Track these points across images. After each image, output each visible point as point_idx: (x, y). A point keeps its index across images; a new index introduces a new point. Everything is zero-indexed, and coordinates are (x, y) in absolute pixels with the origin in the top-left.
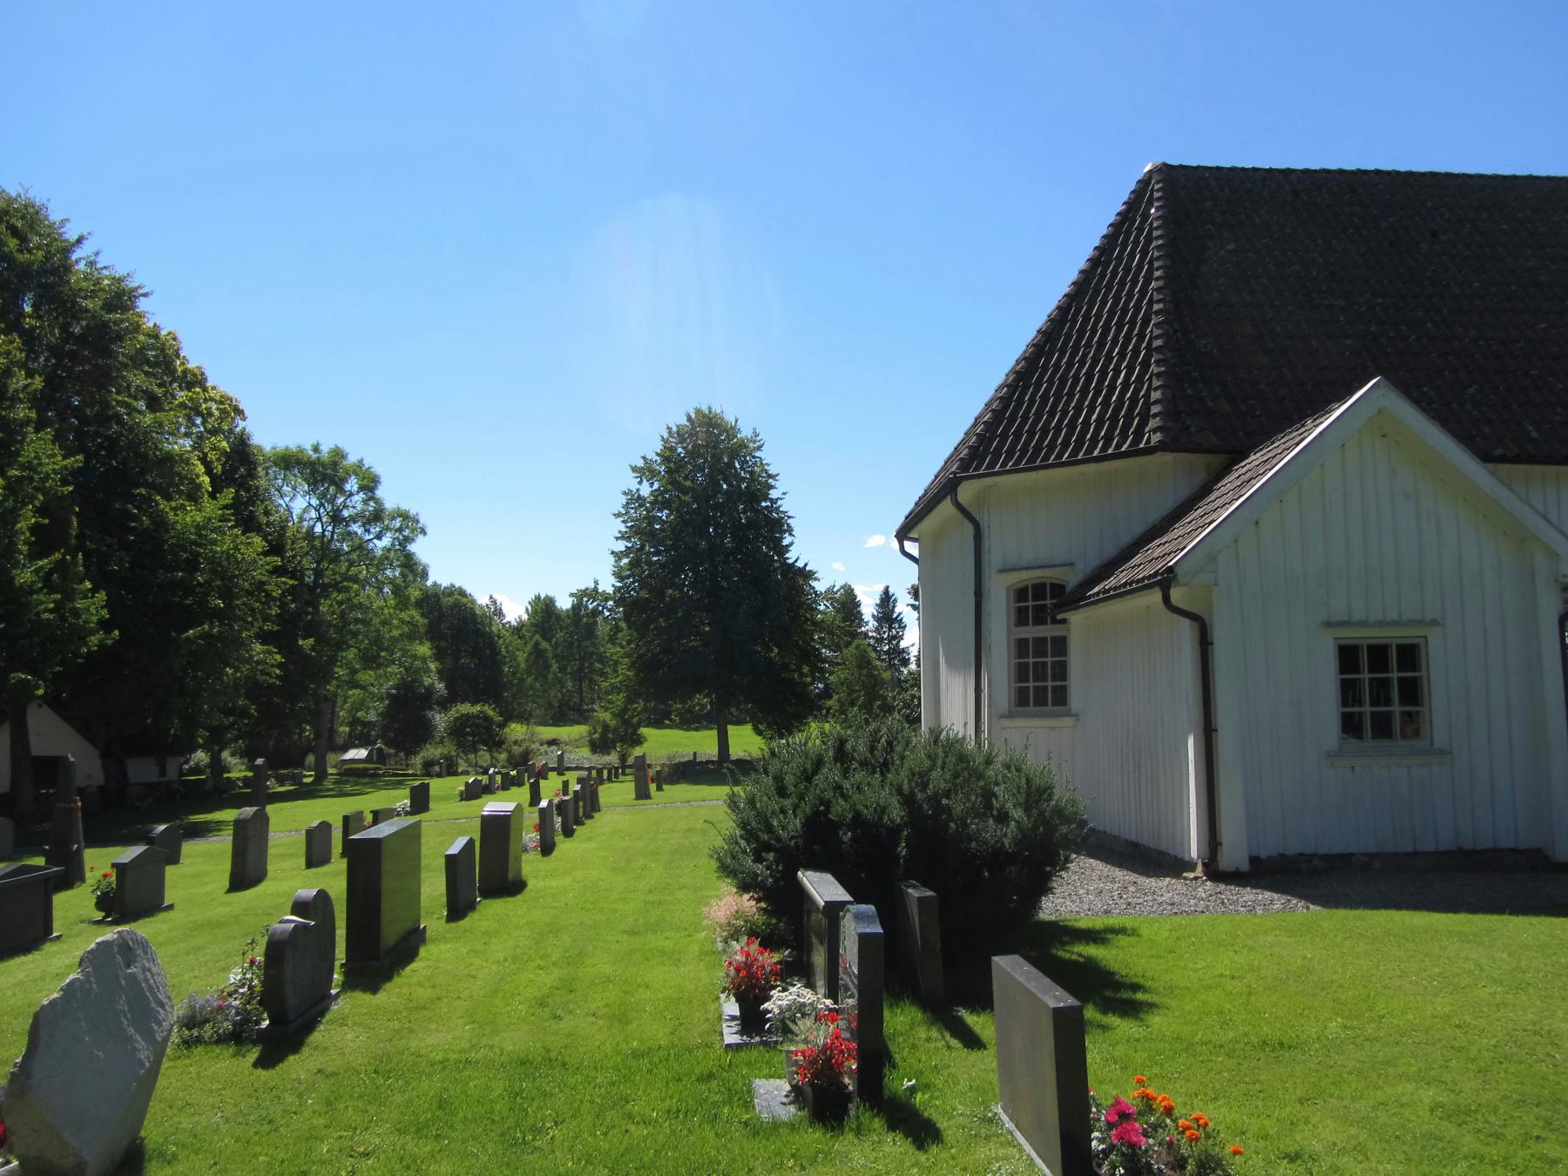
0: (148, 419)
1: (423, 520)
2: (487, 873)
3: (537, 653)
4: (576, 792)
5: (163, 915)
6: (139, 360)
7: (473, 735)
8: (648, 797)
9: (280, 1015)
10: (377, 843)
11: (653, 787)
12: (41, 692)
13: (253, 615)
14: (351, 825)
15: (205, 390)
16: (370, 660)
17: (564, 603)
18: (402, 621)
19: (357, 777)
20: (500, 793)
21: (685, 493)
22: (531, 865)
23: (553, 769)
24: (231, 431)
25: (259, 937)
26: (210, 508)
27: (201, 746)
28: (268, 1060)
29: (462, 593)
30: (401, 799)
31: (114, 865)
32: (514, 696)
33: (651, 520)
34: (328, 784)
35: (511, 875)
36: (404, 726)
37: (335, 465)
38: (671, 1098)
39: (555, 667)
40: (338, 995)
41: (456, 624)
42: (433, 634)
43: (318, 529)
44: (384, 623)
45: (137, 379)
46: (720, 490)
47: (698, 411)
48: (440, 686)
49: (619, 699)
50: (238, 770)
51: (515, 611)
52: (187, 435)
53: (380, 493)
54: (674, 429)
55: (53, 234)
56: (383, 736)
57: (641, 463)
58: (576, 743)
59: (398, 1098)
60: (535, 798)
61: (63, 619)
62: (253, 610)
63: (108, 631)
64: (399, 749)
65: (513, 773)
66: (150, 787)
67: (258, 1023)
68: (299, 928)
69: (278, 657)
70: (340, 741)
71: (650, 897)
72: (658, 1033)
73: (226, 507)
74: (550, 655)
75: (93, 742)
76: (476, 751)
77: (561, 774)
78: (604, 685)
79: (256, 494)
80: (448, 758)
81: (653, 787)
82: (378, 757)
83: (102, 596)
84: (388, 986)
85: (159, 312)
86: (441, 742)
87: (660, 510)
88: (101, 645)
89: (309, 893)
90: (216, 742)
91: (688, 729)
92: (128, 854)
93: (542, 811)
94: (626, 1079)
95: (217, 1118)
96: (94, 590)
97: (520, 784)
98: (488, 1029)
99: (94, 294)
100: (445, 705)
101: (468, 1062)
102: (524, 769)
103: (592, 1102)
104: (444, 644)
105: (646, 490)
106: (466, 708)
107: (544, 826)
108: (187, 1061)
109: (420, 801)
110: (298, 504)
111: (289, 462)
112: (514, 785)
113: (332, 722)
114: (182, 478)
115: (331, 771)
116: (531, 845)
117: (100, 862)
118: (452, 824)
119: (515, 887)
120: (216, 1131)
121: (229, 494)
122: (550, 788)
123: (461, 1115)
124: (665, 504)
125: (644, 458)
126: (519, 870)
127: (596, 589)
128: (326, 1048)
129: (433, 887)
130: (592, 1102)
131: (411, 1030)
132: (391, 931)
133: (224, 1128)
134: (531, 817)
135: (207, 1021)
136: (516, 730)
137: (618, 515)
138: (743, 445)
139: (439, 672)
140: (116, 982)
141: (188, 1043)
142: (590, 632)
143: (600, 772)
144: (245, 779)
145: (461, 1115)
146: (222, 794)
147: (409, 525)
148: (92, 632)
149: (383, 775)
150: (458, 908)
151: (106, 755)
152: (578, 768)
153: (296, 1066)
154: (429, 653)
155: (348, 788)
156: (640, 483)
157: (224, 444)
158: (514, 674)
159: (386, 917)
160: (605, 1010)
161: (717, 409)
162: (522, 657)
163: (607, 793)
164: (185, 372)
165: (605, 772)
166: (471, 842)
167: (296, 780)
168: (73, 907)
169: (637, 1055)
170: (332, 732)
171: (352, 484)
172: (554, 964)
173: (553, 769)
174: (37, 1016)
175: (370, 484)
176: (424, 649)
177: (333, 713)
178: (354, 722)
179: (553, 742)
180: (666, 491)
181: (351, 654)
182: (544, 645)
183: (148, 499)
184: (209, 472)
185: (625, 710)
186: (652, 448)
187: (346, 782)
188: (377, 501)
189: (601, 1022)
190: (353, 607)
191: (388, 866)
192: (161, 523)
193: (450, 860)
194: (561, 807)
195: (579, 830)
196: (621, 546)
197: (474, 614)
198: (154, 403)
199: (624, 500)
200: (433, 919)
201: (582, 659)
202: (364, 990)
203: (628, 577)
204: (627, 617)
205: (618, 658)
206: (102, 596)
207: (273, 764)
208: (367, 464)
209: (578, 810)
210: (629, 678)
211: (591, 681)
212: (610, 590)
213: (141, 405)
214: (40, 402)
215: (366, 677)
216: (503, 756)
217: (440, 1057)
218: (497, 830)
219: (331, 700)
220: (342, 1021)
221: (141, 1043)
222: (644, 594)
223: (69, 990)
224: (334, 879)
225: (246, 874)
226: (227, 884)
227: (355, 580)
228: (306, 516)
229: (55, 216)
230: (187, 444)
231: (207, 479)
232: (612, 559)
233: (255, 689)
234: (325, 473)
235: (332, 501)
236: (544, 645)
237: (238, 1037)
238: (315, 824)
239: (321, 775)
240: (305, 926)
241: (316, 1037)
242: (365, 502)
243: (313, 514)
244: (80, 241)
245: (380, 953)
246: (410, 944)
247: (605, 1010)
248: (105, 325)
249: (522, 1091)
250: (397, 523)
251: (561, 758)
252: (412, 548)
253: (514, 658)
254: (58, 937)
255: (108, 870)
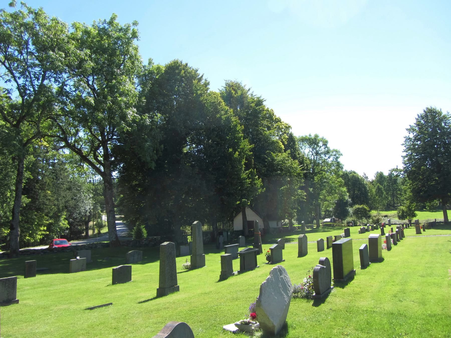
0: (268, 132)
1: (341, 152)
2: (371, 255)
3: (379, 189)
4: (396, 231)
5: (282, 263)
6: (264, 118)
7: (361, 214)
8: (421, 233)
9: (318, 293)
10: (340, 245)
11: (422, 230)
12: (249, 204)
13: (298, 182)
14: (329, 240)
15: (281, 123)
16: (330, 192)
17: (386, 174)
18: (338, 182)
19: (328, 227)
20: (371, 231)
21: (426, 135)
22: (384, 253)
23: (387, 224)
24: (288, 133)
25: (310, 270)
26: (285, 155)
27: (287, 218)
28: (316, 304)
29: (355, 173)
30: (342, 233)
31: (270, 249)
32: (372, 202)
33: (414, 145)
34: (320, 228)
35: (379, 256)
36: (340, 212)
37: (315, 139)
38: (445, 331)
39: (385, 193)
40: (333, 288)
41: (354, 183)
42: (346, 184)
43: (313, 157)
44: (333, 182)
45: (265, 123)
46: (438, 133)
47: (427, 108)
48: (350, 200)
49: (407, 203)
50: (296, 225)
51: (372, 177)
52: (277, 136)
53: (328, 145)
54: (420, 115)
55: (243, 90)
56: (334, 215)
57: (409, 127)
58: (393, 216)
59: (354, 320)
60: (383, 233)
61: (252, 186)
62: (297, 181)
63: (263, 188)
64: (339, 218)
65: (375, 225)
66: (275, 229)
67: (312, 294)
68: (322, 268)
69: (305, 194)
70: (322, 216)
71: (427, 265)
72: (438, 310)
73: (289, 154)
74: (383, 190)
75: (261, 217)
76: (362, 219)
77: (390, 226)
78: (402, 198)
79: (296, 150)
80: (354, 221)
81: (422, 230)
82: (334, 221)
83: (261, 179)
84: (347, 286)
85: (268, 105)
86: (351, 216)
87: (417, 142)
88: (261, 192)
89: (324, 258)
90: (291, 217)
91: (433, 212)
92: (273, 246)
93: (387, 237)
94: (428, 323)
95: (305, 319)
96: (259, 178)
97: (377, 229)
98: (379, 302)
99: (253, 102)
100: (351, 206)
101: (374, 312)
102: (378, 224)
103: (417, 329)
104: (350, 188)
105: (411, 136)
106: (357, 206)
107: (387, 242)
108: (295, 302)
109: (347, 234)
110: (306, 151)
111: (303, 140)
112: (375, 229)
113: (320, 211)
114: (277, 146)
115: (321, 225)
116: (384, 247)
117: (266, 248)
118: (359, 240)
119: (381, 260)
120: (305, 322)
121: (289, 151)
122: (387, 230)
123: (374, 327)
124: (419, 140)
125: (410, 126)
126: (381, 255)
127: (397, 169)
128: (331, 303)
129: (357, 259)
130: (417, 329)
131: (355, 300)
132: (346, 271)
133: (307, 322)
134: (383, 239)
135: (299, 292)
136: (374, 213)
137: (403, 145)
138: (445, 117)
139: (349, 196)
140: (277, 280)
141: (295, 297)
142: (395, 181)
143: (403, 225)
144: (298, 227)
145: (374, 327)
146: (292, 231)
147: (337, 154)
148: (259, 189)
149: (336, 226)
150: (364, 266)
151: (264, 221)
152: (395, 224)
153: (323, 307)
154: (346, 190)
155: (326, 230)
156: (410, 133)
157: (287, 136)
158: (372, 196)
159: (345, 266)
160: (417, 300)
161: (433, 107)
162: (374, 190)
163: (406, 232)
164: (276, 119)
165: (405, 225)
166: (366, 246)
167: (312, 227)
168: (261, 259)
169: (430, 316)
170: (320, 214)
171: (321, 144)
172: (397, 284)
173: (387, 224)
174: (261, 286)
175: (325, 144)
176: (345, 189)
177: (320, 208)
178: (326, 211)
179: (386, 216)
180: (418, 135)
181: (324, 192)
182: (381, 186)
183: (270, 153)
184: (283, 144)
185: (410, 206)
186: (413, 122)
187: (325, 228)
188: (328, 148)
189: (416, 304)
190: (324, 178)
191: (344, 252)
192: (273, 160)
193: (361, 251)
194: (392, 236)
195: (398, 243)
196: (405, 154)
197: (358, 178)
198: (269, 128)
199: (404, 139)
200: (357, 267)
201: (393, 190)
202: (340, 287)
203: (408, 164)
204: (408, 176)
205: (406, 189)
206: (261, 179)
207: (307, 222)
208: (325, 138)
209: (398, 237)
210: (410, 196)
211: (397, 197)
212: (402, 168)
213: (266, 129)
214: (244, 131)
215: (328, 198)
216: (371, 220)
217: (365, 309)
218: (373, 242)
219: (319, 205)
220: (335, 296)
221: (285, 296)
222: (413, 169)
223: (268, 280)
224: (328, 254)
225: (302, 253)
226: (298, 255)
227: (324, 171)
228: (309, 154)
229: (243, 85)
230: (277, 138)
231: (283, 146)
232: (402, 158)
233: (300, 202)
234: (313, 142)
235: (316, 149)
236: (381, 186)
237: (307, 297)
238: (319, 239)
239: (318, 226)
240: (323, 268)
241: (328, 299)
242: (325, 148)
243: (311, 153)
244: (249, 90)
245: (344, 278)
246: (351, 276)
247: (417, 300)
248: (257, 110)
249: (393, 322)
250: (334, 153)
251: (389, 221)
252: (339, 160)
253: (371, 191)
254: (259, 267)
255: (269, 250)
